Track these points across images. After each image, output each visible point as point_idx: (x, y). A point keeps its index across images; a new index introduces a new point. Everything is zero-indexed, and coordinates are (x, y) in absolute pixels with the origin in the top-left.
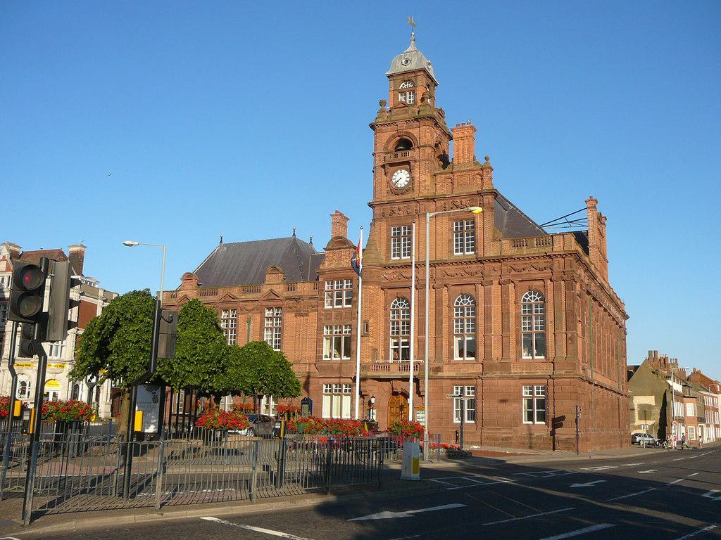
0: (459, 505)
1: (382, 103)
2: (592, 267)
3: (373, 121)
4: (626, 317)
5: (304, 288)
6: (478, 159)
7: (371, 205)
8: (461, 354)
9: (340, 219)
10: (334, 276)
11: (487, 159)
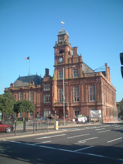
0: (97, 137)
1: (56, 42)
2: (23, 88)
3: (54, 46)
4: (116, 91)
5: (39, 86)
6: (79, 55)
7: (54, 66)
8: (76, 101)
9: (47, 71)
10: (45, 83)
11: (81, 55)
